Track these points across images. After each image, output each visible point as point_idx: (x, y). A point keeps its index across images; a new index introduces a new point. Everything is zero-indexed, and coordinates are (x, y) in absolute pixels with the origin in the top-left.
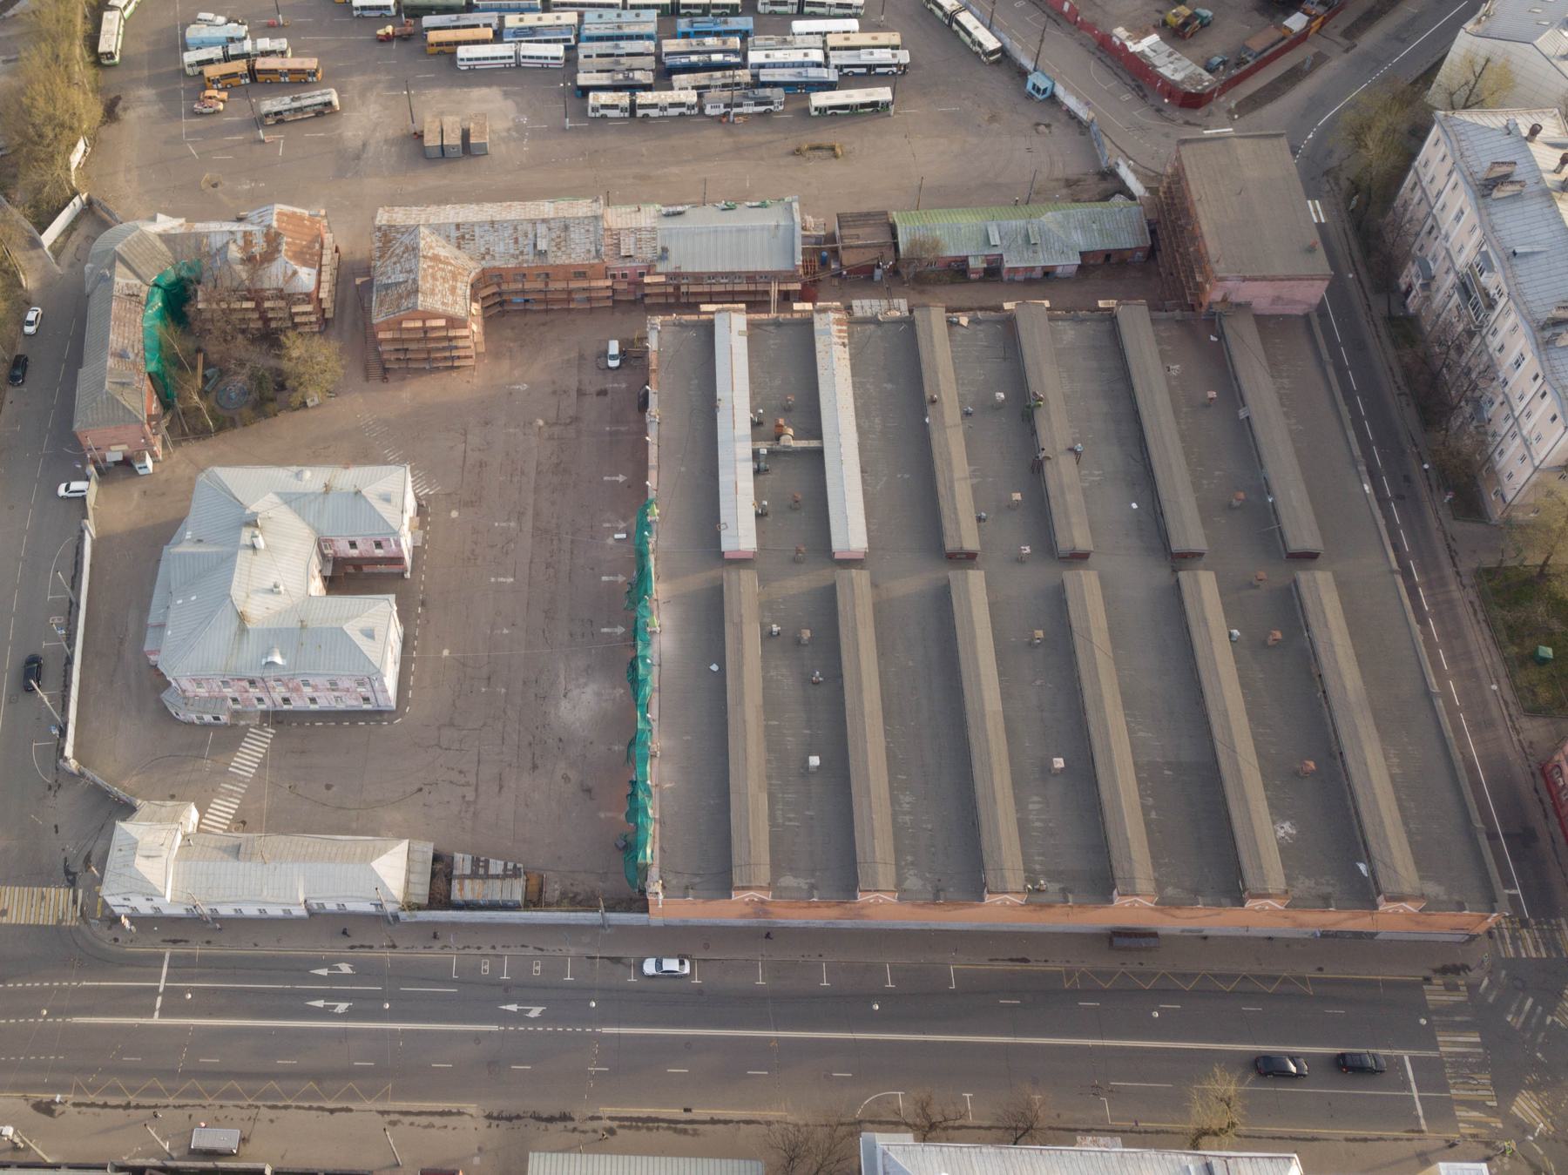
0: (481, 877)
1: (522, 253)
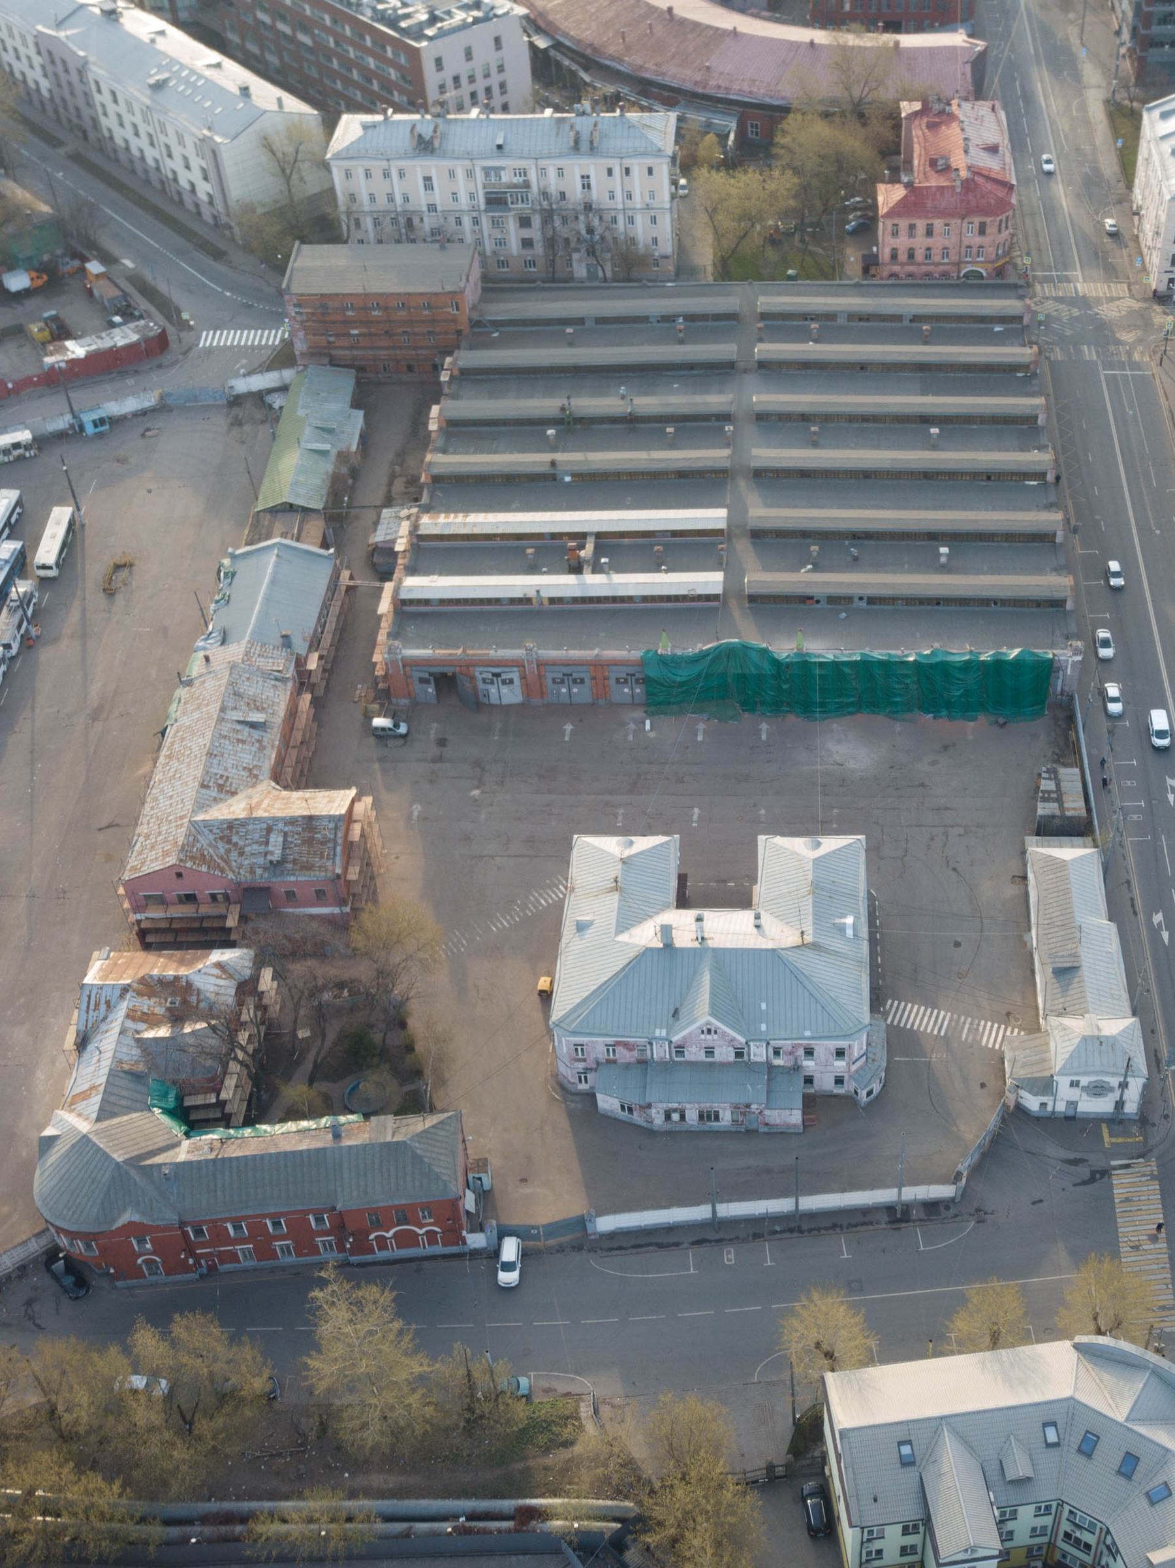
1: (258, 741)
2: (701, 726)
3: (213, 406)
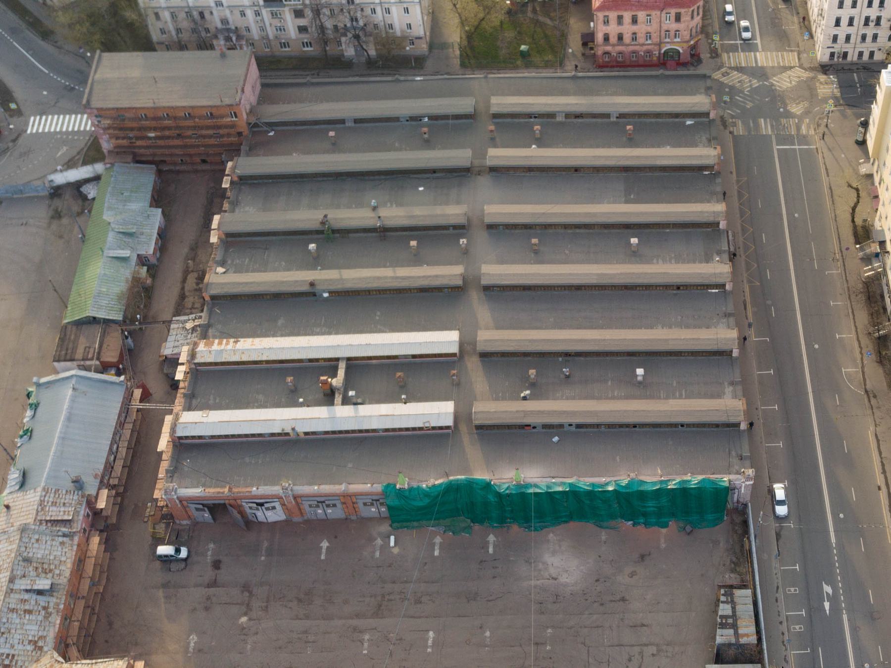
0: (735, 621)
1: (45, 608)
2: (438, 540)
3: (37, 197)
